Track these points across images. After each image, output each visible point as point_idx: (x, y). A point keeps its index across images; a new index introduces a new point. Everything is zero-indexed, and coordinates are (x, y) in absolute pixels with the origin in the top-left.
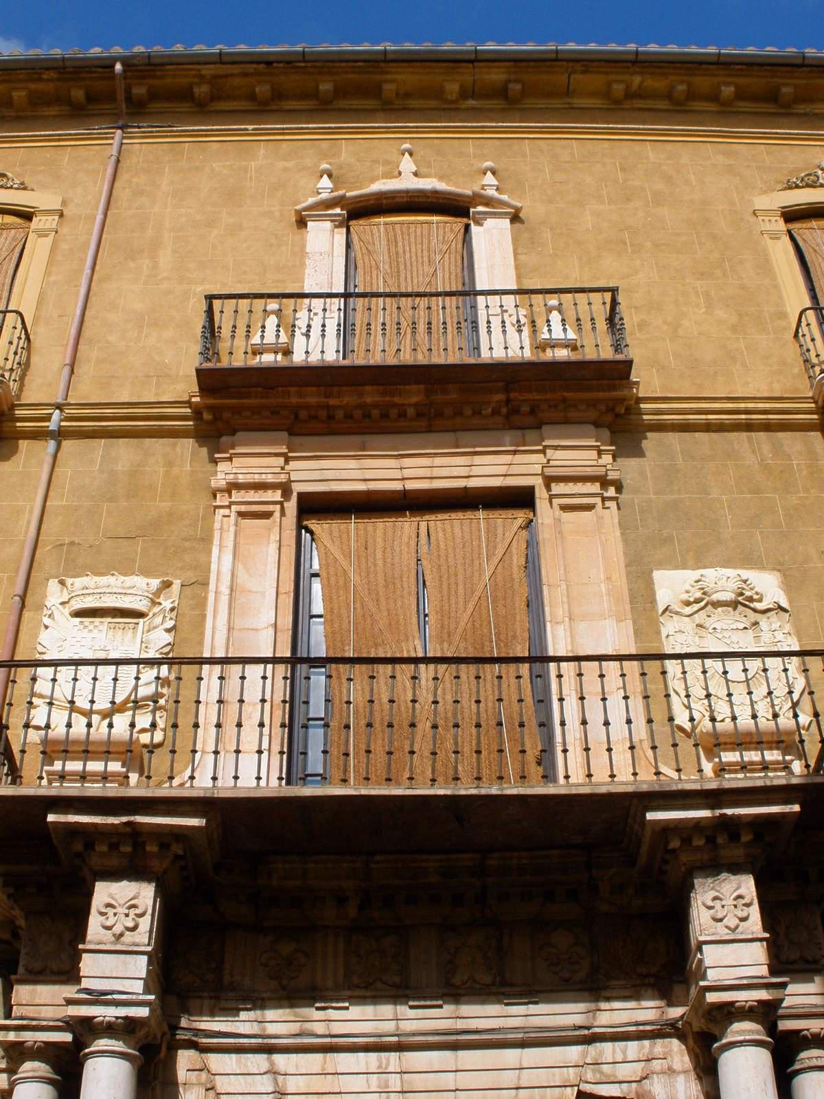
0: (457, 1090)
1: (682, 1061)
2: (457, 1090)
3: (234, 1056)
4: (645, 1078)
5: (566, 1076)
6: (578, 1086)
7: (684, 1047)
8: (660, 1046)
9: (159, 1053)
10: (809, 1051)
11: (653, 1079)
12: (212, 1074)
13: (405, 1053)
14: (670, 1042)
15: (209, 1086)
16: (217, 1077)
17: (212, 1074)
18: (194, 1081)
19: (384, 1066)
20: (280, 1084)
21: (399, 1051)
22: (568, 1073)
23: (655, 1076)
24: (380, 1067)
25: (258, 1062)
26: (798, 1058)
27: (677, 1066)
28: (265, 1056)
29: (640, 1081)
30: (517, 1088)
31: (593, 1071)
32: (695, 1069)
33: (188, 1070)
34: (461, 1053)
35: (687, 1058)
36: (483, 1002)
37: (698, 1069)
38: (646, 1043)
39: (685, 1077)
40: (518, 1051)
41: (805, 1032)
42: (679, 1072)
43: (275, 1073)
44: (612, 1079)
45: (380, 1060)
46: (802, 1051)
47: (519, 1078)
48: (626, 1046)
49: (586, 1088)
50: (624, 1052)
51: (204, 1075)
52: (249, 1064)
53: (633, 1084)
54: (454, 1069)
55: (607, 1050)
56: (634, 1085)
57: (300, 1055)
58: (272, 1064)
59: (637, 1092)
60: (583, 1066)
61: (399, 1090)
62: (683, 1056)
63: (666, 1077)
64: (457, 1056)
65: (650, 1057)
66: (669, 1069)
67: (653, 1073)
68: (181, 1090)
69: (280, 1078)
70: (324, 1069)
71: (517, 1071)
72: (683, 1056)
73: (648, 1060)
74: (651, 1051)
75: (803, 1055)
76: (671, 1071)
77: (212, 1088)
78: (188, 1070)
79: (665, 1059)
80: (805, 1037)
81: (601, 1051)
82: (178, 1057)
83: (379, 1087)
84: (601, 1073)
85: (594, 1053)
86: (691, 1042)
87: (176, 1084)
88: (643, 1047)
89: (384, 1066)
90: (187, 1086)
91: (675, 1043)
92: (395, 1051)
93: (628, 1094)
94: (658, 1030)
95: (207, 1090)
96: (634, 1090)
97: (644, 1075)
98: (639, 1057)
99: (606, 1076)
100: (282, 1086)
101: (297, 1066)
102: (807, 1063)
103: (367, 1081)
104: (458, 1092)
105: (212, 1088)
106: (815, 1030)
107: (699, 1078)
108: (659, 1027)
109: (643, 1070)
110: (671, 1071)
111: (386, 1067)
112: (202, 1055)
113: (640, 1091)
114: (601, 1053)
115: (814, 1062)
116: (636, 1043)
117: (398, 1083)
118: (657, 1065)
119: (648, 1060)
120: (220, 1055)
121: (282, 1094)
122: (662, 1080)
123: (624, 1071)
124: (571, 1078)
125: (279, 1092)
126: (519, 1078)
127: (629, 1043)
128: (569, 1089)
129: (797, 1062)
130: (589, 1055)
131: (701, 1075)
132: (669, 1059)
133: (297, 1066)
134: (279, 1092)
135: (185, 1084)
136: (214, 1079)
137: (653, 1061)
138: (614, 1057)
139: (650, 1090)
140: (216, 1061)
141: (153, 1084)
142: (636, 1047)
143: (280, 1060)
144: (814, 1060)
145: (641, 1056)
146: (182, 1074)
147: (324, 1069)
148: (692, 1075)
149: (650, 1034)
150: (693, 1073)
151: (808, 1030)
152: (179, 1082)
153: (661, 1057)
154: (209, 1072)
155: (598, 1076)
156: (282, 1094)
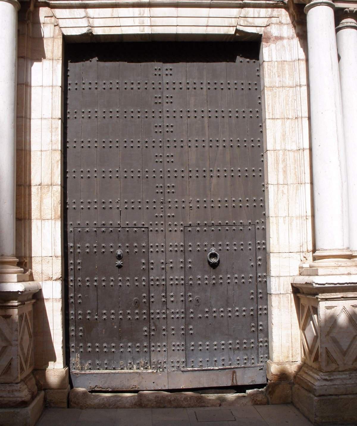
0: (177, 26)
1: (287, 20)
2: (177, 26)
3: (68, 10)
4: (268, 26)
5: (231, 22)
6: (236, 26)
7: (287, 13)
8: (276, 12)
9: (29, 7)
10: (347, 19)
11: (272, 27)
12: (57, 19)
13: (152, 8)
14: (281, 10)
15: (56, 24)
16: (59, 20)
17: (57, 19)
18: (49, 22)
19: (142, 14)
20: (91, 23)
21: (149, 7)
22: (232, 21)
23: (273, 25)
24: (140, 14)
25: (81, 12)
26: (341, 22)
27: (284, 21)
28: (83, 10)
29: (265, 27)
30: (207, 26)
31: (244, 20)
32: (292, 23)
33: (45, 17)
34: (180, 9)
35: (288, 18)
36: (177, 35)
37: (294, 22)
38: (270, 10)
39: (287, 26)
40: (208, 9)
41: (347, 9)
42: (285, 24)
43: (88, 17)
44: (252, 25)
45: (140, 11)
46: (343, 19)
47: (208, 22)
48: (260, 10)
49: (239, 28)
50: (259, 13)
51: (53, 19)
52: (75, 13)
53: (262, 28)
54: (176, 16)
55: (251, 11)
56: (263, 28)
57: (100, 9)
58: (87, 13)
59: (264, 32)
60: (239, 18)
61: (149, 25)
62: (287, 17)
63: (278, 25)
64: (178, 10)
65: (271, 16)
66: (280, 22)
67: (272, 24)
68: (42, 26)
69: (91, 20)
70: (112, 15)
71: (207, 18)
72: (287, 17)
73: (270, 18)
74: (271, 14)
75: (344, 21)
76: (281, 23)
77: (57, 25)
78: (45, 17)
79: (278, 17)
80: (346, 11)
81: (247, 12)
82: (40, 11)
83: (140, 23)
84: (247, 21)
85: (244, 12)
86: (292, 9)
87: (40, 23)
88: (268, 12)
89: (142, 14)
90: (45, 24)
91: (283, 11)
92: (148, 7)
93: (260, 32)
94: (276, 3)
95: (55, 26)
96: (263, 31)
97: (268, 24)
98: (266, 16)
99: (251, 23)
100: (92, 23)
101: (99, 14)
102: (345, 25)
103: (134, 21)
104: (178, 27)
105: (57, 25)
106: (352, 9)
107: (295, 27)
108: (276, 2)
109: (267, 22)
110: (281, 23)
111: (143, 15)
112: (52, 10)
113: (266, 31)
114: (248, 13)
115: (349, 24)
116: (264, 9)
117: (149, 21)
118: (274, 20)
119: (270, 18)
120: (32, 132)
121: (92, 27)
122: (276, 27)
123: (258, 22)
124: (233, 23)
125: (90, 26)
126: (208, 22)
127: (262, 9)
128: (232, 28)
129: (340, 24)
130: (242, 13)
131: (296, 25)
132: (280, 18)
133: (99, 14)
134: (90, 26)
135: (44, 23)
136: (58, 21)
137: (272, 18)
138: (254, 15)
139: (270, 31)
140: (59, 12)
141: (28, 22)
142: (265, 11)
143: (91, 12)
144: (349, 23)
145: (267, 15)
146: (42, 19)
147: (112, 15)
148: (291, 26)
149: (272, 6)
150: (291, 25)
151: (348, 8)
152: (41, 22)
153: (276, 16)
154: (55, 17)
155: (246, 23)
156: (92, 27)
